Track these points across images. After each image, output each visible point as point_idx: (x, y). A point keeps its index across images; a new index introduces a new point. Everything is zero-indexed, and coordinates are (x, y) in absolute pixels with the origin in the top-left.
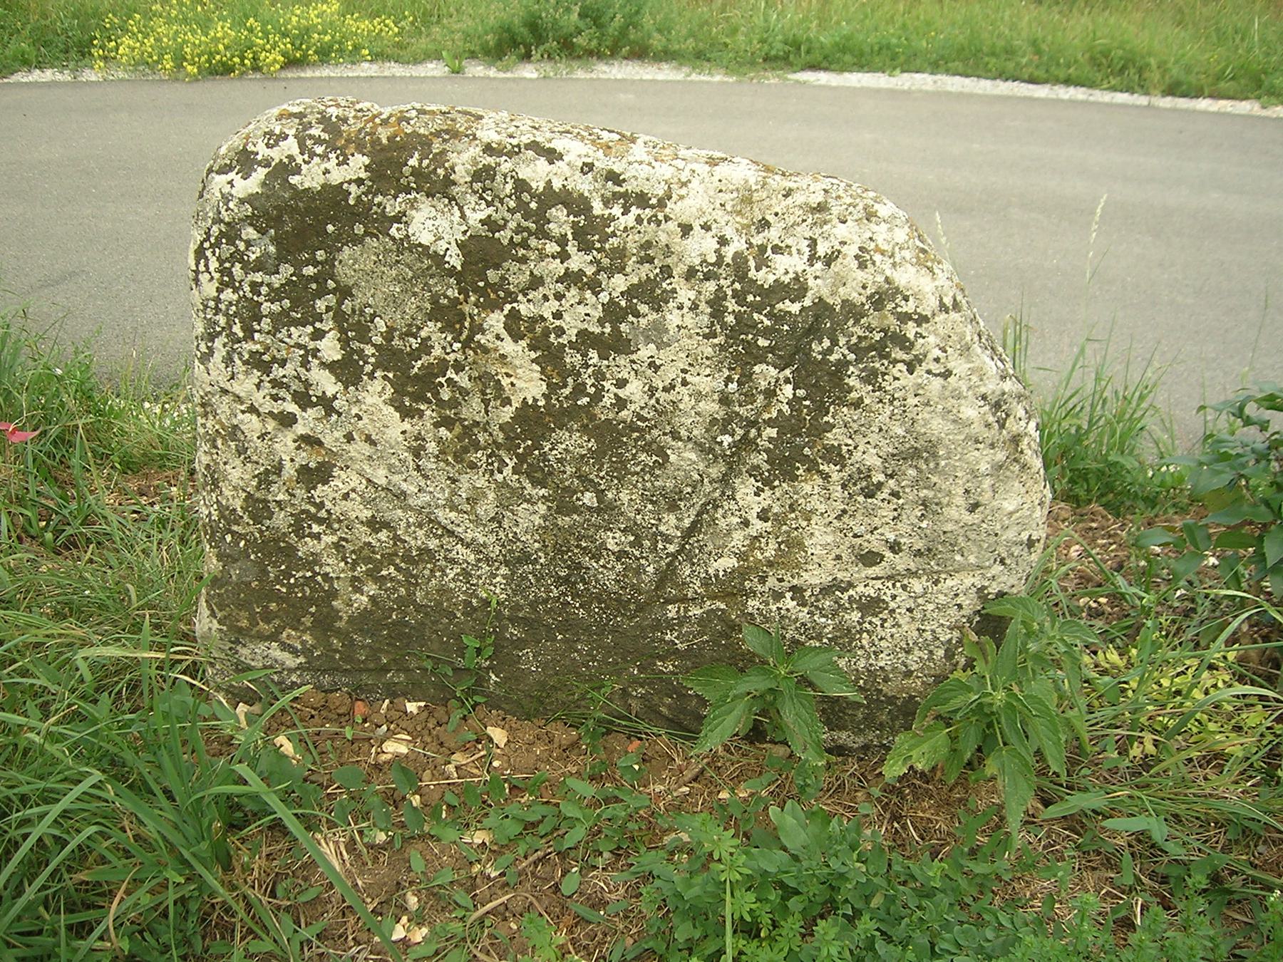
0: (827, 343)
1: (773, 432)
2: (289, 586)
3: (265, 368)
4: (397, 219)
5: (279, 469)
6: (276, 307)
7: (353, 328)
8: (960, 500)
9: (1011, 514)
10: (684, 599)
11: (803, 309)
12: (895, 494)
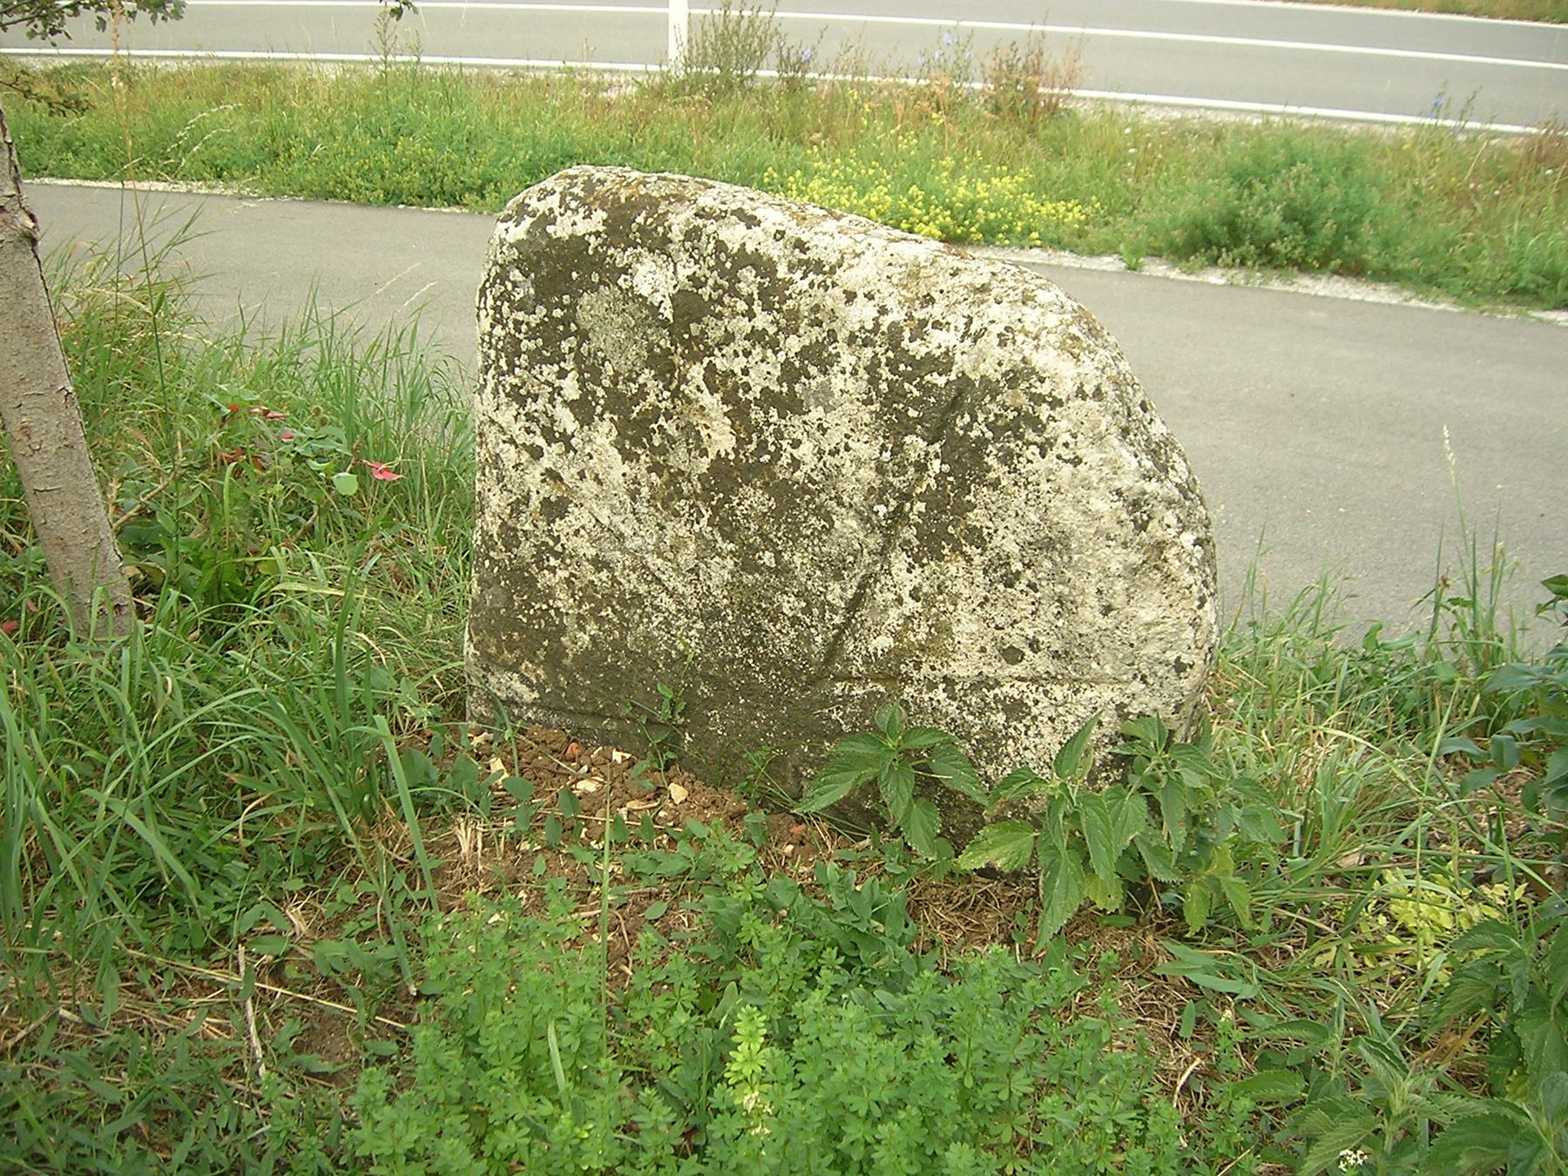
2: (530, 617)
4: (624, 271)
6: (532, 345)
7: (589, 370)
8: (1092, 600)
9: (1149, 625)
11: (948, 382)
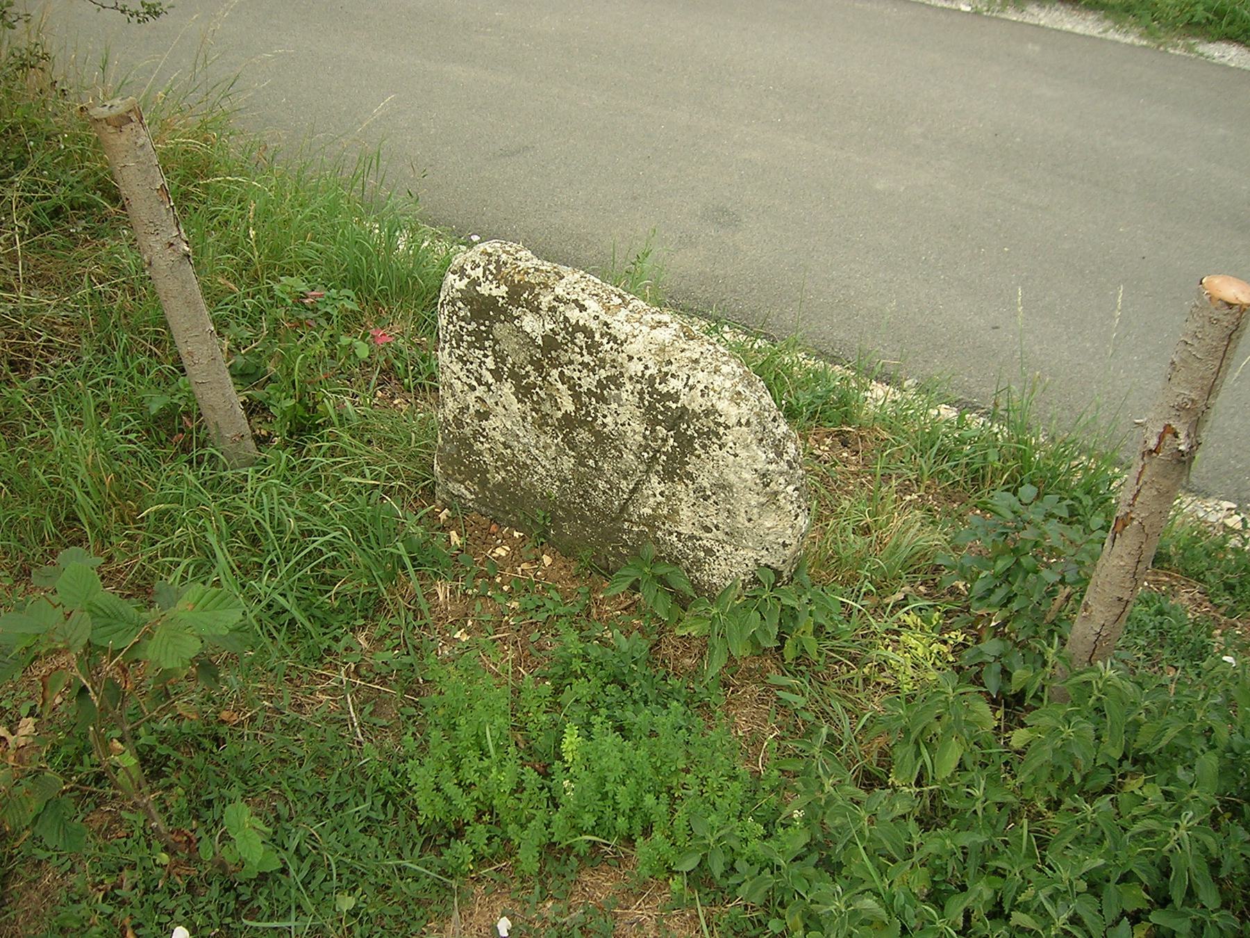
5: (468, 408)
7: (500, 358)
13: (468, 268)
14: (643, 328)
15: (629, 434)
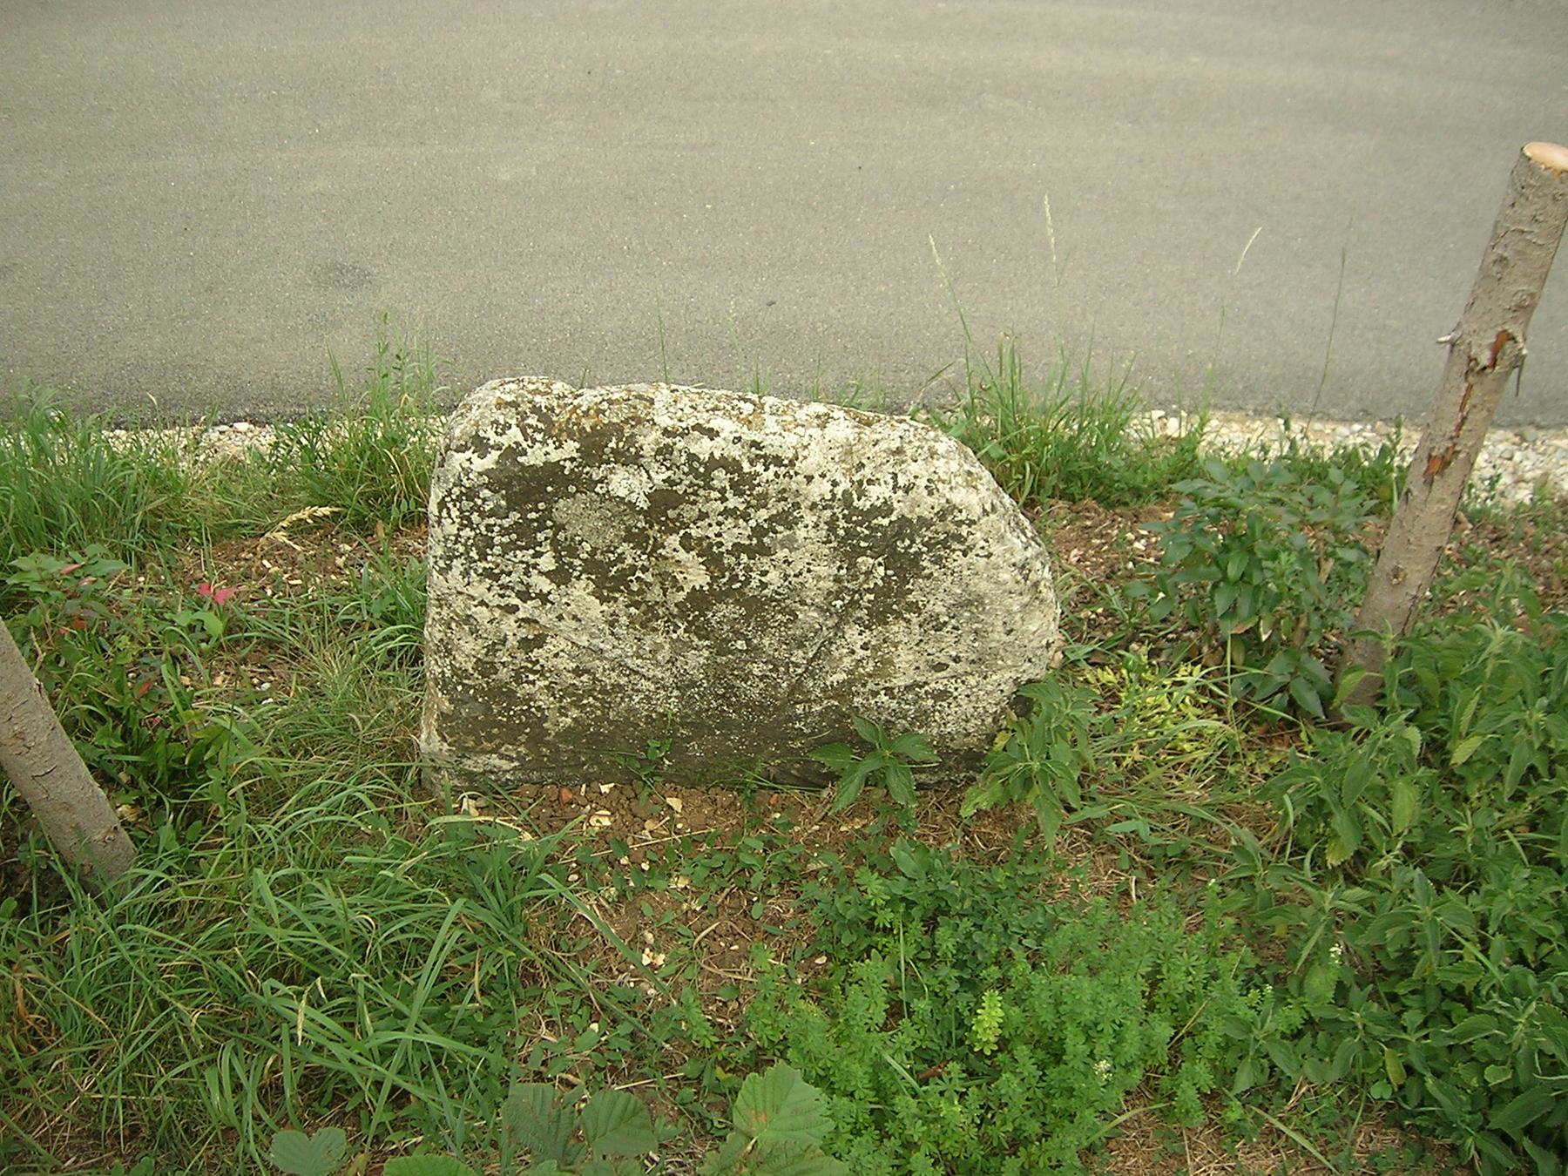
0: (907, 542)
1: (872, 597)
3: (496, 578)
5: (504, 641)
6: (505, 539)
8: (1000, 629)
10: (809, 701)
12: (957, 628)
13: (491, 434)
14: (811, 431)
15: (811, 583)
